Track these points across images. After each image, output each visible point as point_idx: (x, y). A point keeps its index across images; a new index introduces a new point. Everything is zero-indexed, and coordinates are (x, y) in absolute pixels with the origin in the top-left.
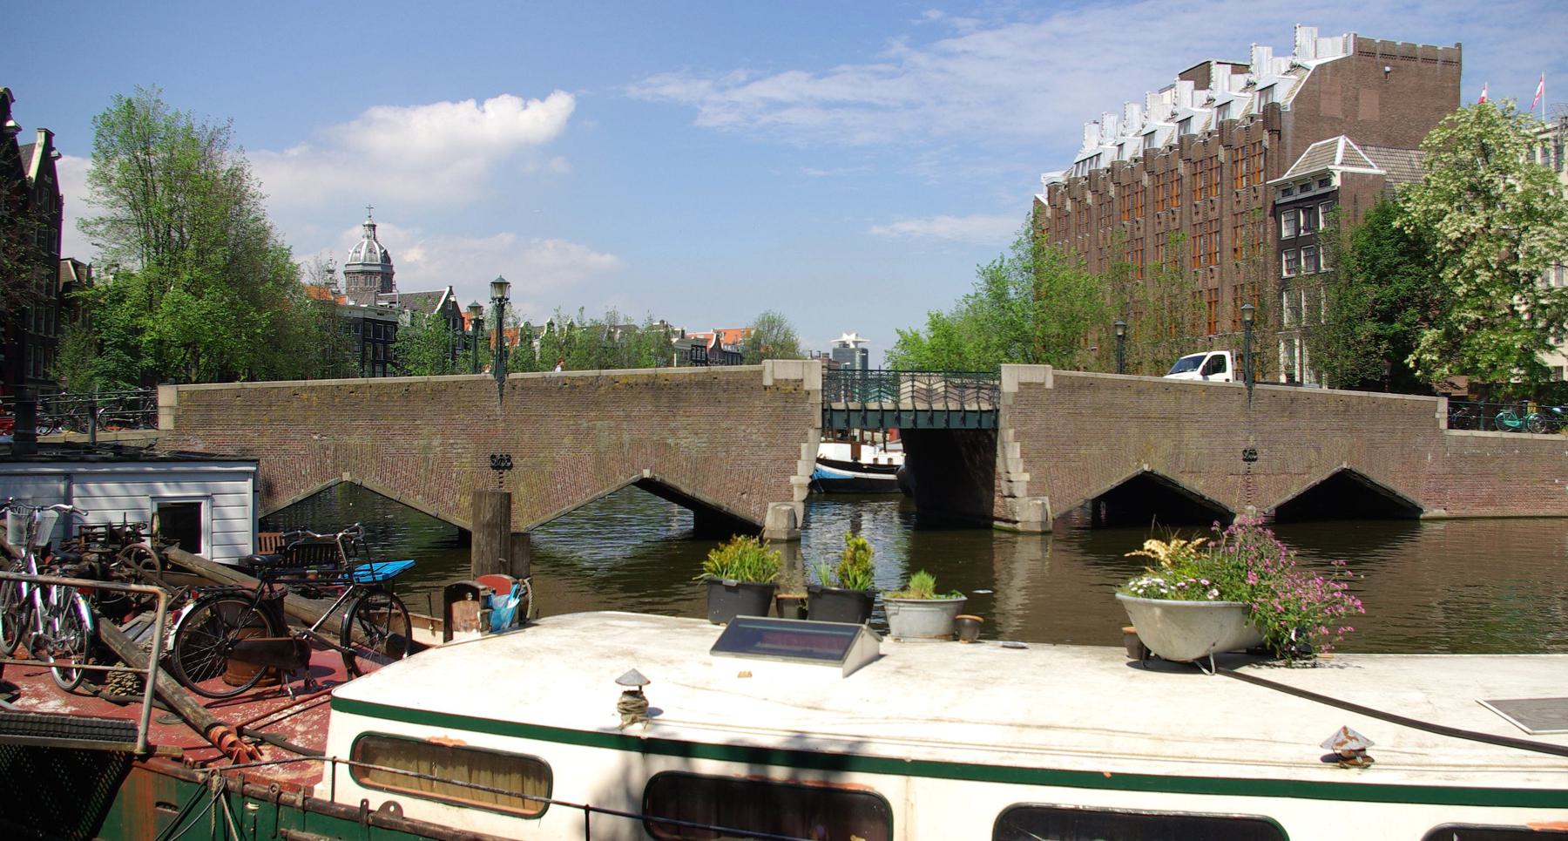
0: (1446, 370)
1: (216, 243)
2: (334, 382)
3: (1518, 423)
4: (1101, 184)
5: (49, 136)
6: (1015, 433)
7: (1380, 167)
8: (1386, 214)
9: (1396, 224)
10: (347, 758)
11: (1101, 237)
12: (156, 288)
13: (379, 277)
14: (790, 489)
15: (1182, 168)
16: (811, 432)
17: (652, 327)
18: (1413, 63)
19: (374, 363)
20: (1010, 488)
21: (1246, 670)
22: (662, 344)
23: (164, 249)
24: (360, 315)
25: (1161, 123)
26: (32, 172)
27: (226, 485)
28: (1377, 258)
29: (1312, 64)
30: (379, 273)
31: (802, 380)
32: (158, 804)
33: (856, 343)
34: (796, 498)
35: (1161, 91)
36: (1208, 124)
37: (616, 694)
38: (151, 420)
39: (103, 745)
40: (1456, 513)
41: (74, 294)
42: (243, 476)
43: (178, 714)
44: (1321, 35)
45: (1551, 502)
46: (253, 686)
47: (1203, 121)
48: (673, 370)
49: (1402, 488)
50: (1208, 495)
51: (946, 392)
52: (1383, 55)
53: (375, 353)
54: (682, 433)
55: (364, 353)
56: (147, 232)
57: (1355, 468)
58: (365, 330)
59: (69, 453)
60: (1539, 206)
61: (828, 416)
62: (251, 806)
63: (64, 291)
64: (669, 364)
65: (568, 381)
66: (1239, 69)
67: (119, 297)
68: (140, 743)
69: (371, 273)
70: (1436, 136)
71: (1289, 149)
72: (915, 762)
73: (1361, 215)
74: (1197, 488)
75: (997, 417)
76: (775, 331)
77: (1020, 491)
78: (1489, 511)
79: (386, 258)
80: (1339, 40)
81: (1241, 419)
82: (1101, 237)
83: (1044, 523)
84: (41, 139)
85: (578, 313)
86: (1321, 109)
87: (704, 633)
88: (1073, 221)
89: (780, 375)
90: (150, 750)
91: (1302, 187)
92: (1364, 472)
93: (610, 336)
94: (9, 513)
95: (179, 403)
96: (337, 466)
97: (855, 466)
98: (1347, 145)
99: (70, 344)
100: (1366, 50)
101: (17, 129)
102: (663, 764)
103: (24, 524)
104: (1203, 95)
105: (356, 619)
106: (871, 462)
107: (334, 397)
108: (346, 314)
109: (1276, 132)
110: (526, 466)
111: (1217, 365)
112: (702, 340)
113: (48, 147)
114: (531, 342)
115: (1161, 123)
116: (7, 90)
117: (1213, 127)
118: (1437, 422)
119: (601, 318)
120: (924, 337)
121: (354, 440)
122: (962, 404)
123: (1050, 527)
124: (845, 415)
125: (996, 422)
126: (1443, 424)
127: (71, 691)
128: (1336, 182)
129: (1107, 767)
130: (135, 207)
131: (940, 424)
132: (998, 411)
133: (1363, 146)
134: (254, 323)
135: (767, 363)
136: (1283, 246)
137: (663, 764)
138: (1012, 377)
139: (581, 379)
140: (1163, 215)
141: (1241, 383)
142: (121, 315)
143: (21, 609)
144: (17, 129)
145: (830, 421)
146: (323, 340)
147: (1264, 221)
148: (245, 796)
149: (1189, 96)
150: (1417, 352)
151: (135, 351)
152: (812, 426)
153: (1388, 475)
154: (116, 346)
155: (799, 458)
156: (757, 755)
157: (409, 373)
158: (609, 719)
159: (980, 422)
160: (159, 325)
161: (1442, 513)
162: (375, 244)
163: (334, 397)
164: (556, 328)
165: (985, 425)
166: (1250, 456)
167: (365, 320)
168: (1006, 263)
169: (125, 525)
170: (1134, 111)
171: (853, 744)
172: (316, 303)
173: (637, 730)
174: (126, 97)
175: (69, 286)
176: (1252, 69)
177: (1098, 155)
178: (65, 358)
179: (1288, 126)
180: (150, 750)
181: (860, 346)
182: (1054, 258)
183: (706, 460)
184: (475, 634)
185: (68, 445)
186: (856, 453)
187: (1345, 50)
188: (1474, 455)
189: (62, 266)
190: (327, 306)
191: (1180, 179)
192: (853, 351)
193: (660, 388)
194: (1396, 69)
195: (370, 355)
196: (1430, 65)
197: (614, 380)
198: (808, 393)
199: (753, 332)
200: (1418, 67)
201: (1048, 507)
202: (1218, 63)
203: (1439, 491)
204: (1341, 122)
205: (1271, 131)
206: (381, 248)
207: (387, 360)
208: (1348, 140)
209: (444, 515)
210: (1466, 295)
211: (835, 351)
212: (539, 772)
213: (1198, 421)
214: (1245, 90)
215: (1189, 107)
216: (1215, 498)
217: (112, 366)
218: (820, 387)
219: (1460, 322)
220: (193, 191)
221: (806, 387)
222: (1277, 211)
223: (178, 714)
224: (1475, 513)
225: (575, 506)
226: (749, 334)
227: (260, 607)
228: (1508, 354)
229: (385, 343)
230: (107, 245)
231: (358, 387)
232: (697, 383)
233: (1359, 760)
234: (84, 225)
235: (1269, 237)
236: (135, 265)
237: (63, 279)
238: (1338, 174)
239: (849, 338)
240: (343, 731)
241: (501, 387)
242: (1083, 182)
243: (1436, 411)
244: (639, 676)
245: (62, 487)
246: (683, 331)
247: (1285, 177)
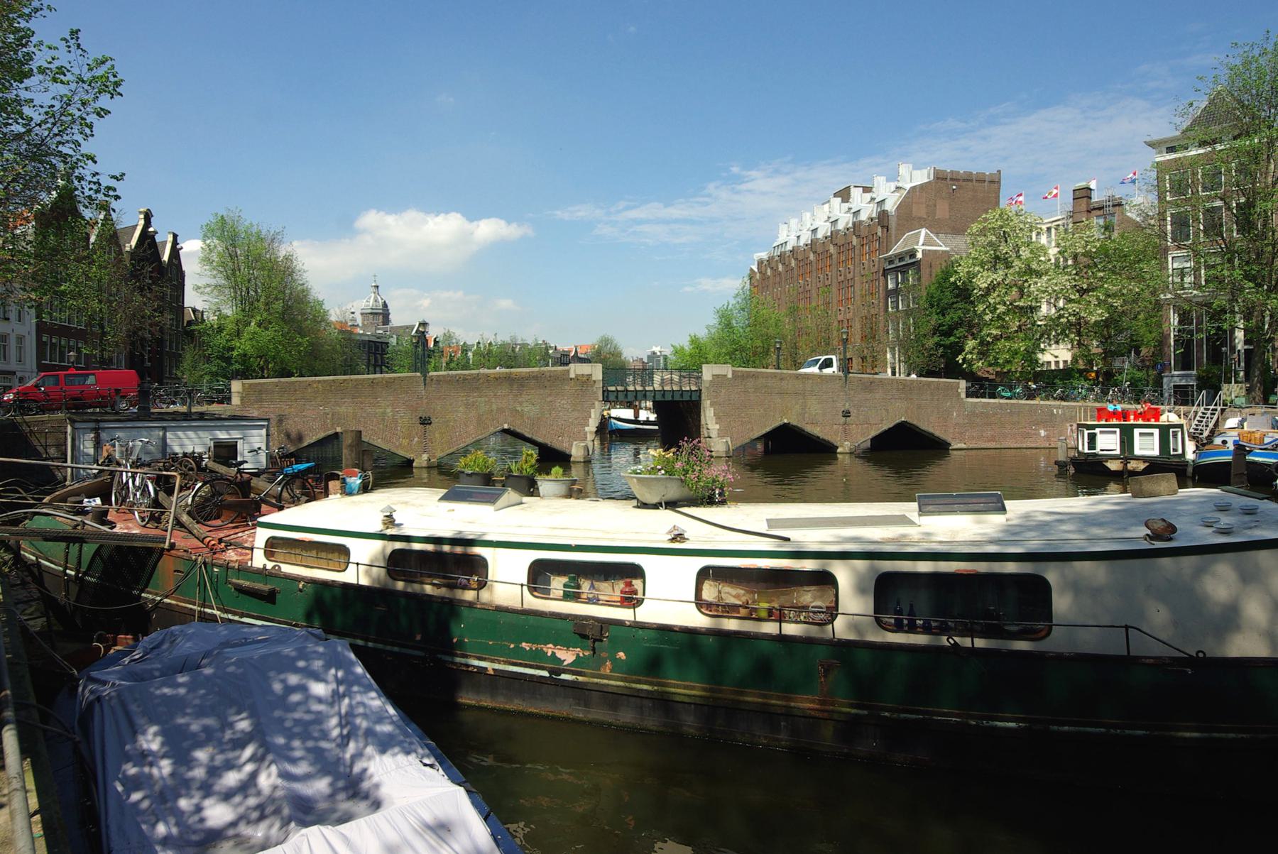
0: (980, 364)
1: (277, 299)
2: (331, 378)
3: (1009, 394)
4: (787, 259)
5: (175, 236)
7: (946, 246)
8: (947, 274)
9: (952, 280)
10: (263, 546)
11: (787, 290)
12: (242, 323)
13: (381, 317)
14: (585, 434)
15: (832, 249)
16: (597, 403)
17: (537, 344)
18: (970, 183)
19: (375, 366)
20: (708, 433)
21: (685, 510)
22: (544, 354)
23: (247, 304)
24: (367, 338)
25: (822, 223)
26: (166, 258)
27: (255, 432)
28: (940, 300)
29: (908, 186)
30: (381, 314)
32: (175, 571)
33: (660, 352)
34: (588, 439)
35: (823, 204)
36: (847, 223)
37: (381, 517)
38: (229, 400)
39: (150, 545)
40: (971, 446)
41: (193, 328)
42: (261, 427)
43: (191, 533)
44: (914, 169)
45: (1030, 439)
46: (231, 523)
47: (845, 221)
48: (550, 368)
49: (938, 433)
50: (821, 436)
52: (951, 179)
53: (376, 360)
54: (525, 404)
55: (369, 360)
56: (236, 292)
57: (910, 420)
58: (370, 348)
59: (161, 417)
60: (1034, 266)
61: (606, 394)
62: (216, 570)
63: (187, 326)
64: (548, 365)
66: (867, 190)
67: (220, 329)
68: (167, 544)
69: (376, 314)
70: (975, 227)
71: (893, 237)
72: (497, 542)
73: (934, 275)
75: (700, 394)
76: (609, 346)
77: (714, 434)
78: (993, 445)
79: (385, 305)
80: (925, 172)
82: (787, 290)
83: (727, 452)
84: (170, 238)
85: (494, 337)
87: (437, 493)
88: (771, 281)
89: (579, 372)
90: (172, 546)
91: (890, 262)
92: (915, 423)
93: (513, 350)
94: (117, 443)
95: (244, 390)
96: (333, 424)
97: (636, 421)
98: (926, 233)
99: (188, 356)
101: (156, 233)
102: (398, 545)
103: (124, 449)
104: (846, 206)
105: (285, 490)
106: (645, 419)
107: (331, 386)
108: (358, 338)
109: (886, 228)
110: (438, 423)
111: (828, 364)
113: (175, 243)
114: (467, 354)
115: (822, 223)
116: (148, 210)
117: (850, 225)
118: (959, 394)
119: (507, 339)
120: (687, 348)
121: (343, 410)
122: (681, 387)
123: (731, 454)
124: (615, 394)
125: (700, 397)
126: (963, 395)
127: (144, 526)
128: (919, 255)
129: (573, 543)
130: (228, 278)
131: (668, 398)
132: (701, 390)
133: (937, 234)
134: (300, 344)
135: (572, 366)
136: (889, 293)
137: (398, 545)
138: (708, 372)
139: (469, 375)
140: (821, 276)
141: (841, 374)
142: (220, 340)
143: (122, 489)
144: (156, 233)
145: (607, 397)
146: (344, 353)
147: (879, 279)
148: (213, 565)
149: (838, 207)
150: (963, 354)
151: (228, 360)
152: (597, 400)
153: (929, 424)
154: (217, 357)
156: (438, 541)
157: (395, 372)
158: (377, 527)
159: (691, 397)
160: (243, 345)
161: (963, 446)
163: (331, 386)
164: (481, 345)
165: (693, 399)
166: (846, 414)
167: (370, 341)
168: (730, 307)
169: (194, 453)
170: (807, 216)
171: (480, 536)
172: (341, 332)
173: (389, 532)
174: (220, 214)
175: (190, 323)
176: (874, 190)
177: (786, 243)
178: (187, 363)
179: (893, 224)
180: (172, 546)
181: (663, 353)
182: (758, 303)
183: (538, 419)
184: (339, 496)
185: (175, 413)
186: (637, 415)
187: (929, 177)
188: (982, 413)
189: (185, 312)
190: (346, 334)
191: (831, 256)
192: (659, 356)
193: (513, 380)
194: (960, 187)
195: (373, 362)
198: (595, 382)
201: (730, 443)
202: (855, 187)
203: (961, 433)
204: (925, 220)
205: (882, 227)
207: (383, 364)
209: (394, 450)
210: (991, 320)
211: (649, 357)
212: (344, 551)
214: (869, 202)
215: (838, 213)
216: (826, 438)
217: (214, 369)
218: (601, 378)
219: (988, 336)
220: (263, 269)
221: (594, 378)
222: (885, 273)
223: (191, 533)
224: (983, 446)
225: (466, 444)
226: (594, 348)
227: (236, 484)
228: (1016, 354)
229: (382, 355)
230: (211, 299)
231: (345, 380)
232: (533, 377)
233: (678, 539)
234: (197, 288)
235: (881, 289)
236: (228, 311)
237: (186, 319)
238: (920, 251)
239: (657, 349)
240: (262, 536)
241: (425, 380)
242: (777, 258)
243: (958, 388)
244: (392, 508)
245: (161, 433)
247: (890, 253)
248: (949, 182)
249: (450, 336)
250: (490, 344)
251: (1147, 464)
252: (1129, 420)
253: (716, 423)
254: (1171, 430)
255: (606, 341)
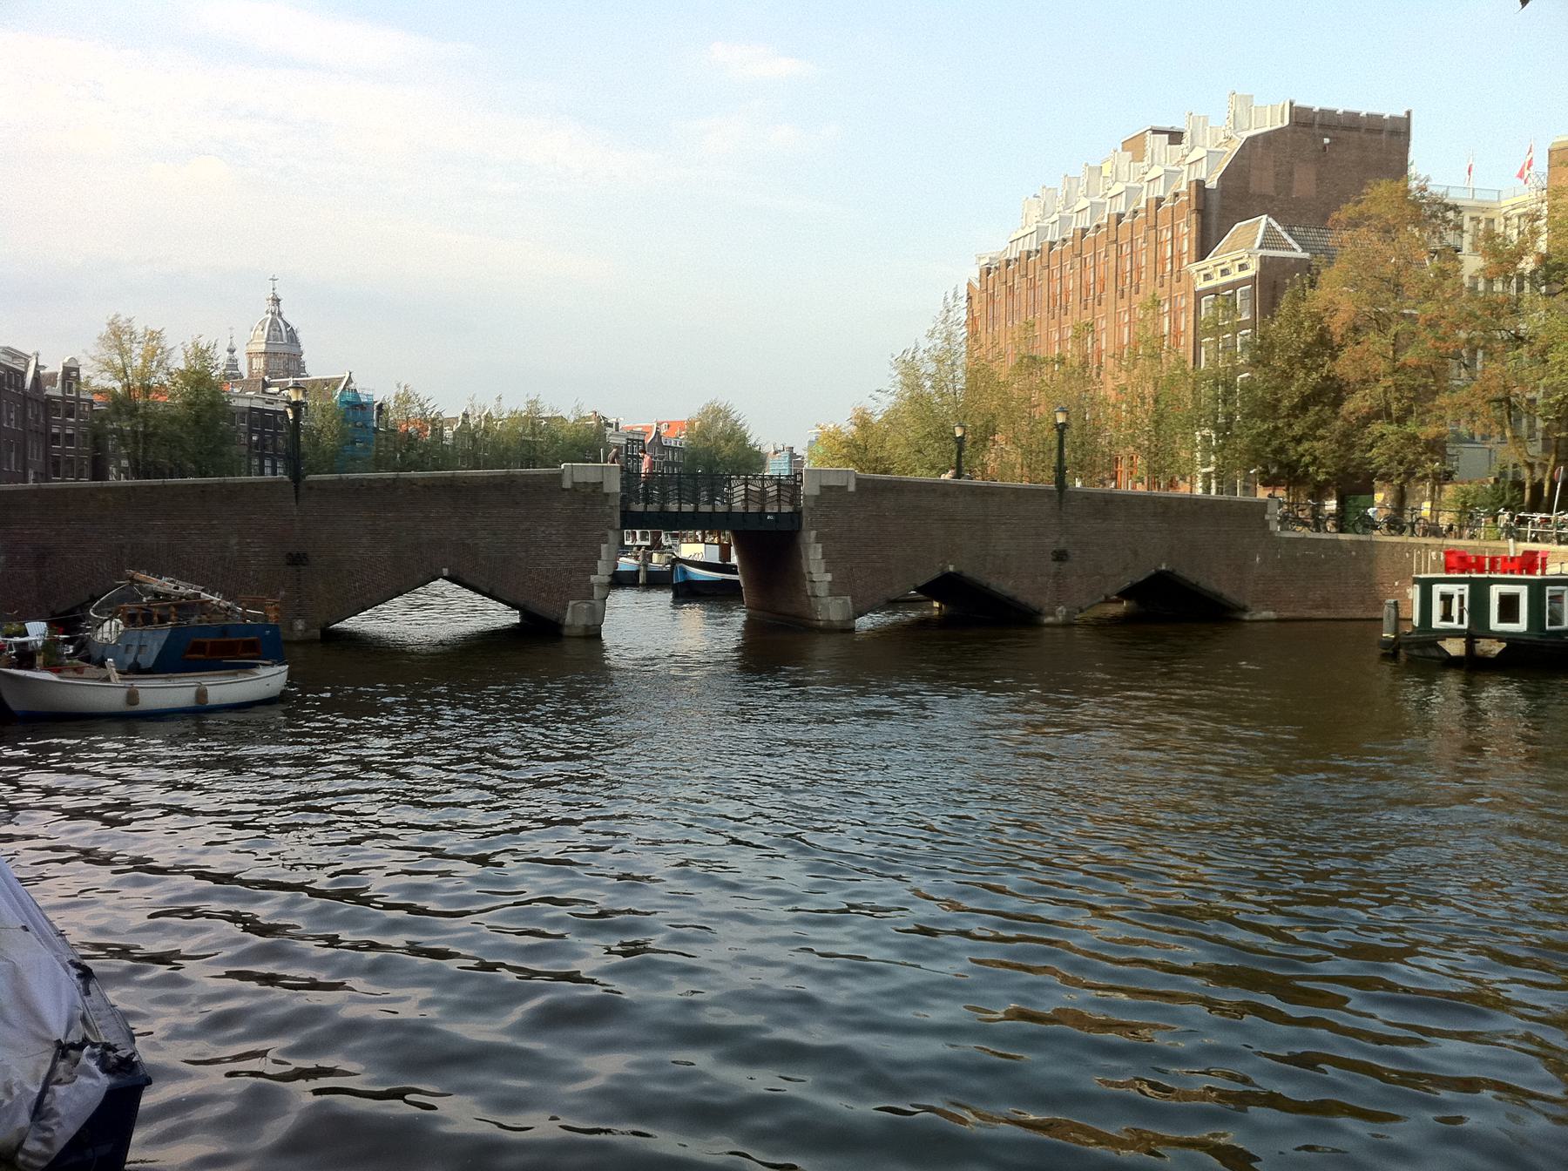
6: (817, 534)
7: (1304, 250)
18: (1355, 135)
31: (602, 483)
51: (779, 495)
52: (1322, 126)
65: (365, 483)
74: (1004, 588)
77: (822, 591)
81: (1053, 521)
86: (1251, 185)
89: (579, 478)
98: (1268, 226)
100: (1303, 121)
112: (639, 433)
149: (1126, 168)
152: (612, 528)
155: (599, 558)
162: (280, 321)
194: (1336, 141)
196: (1374, 137)
197: (411, 482)
199: (697, 424)
200: (1360, 138)
206: (287, 325)
208: (1270, 220)
213: (1005, 524)
221: (606, 490)
241: (297, 488)
243: (1266, 512)
246: (617, 424)
248: (1317, 131)
249: (408, 400)
250: (488, 418)
251: (1504, 645)
252: (1534, 574)
253: (827, 571)
254: (1548, 588)
255: (718, 413)
